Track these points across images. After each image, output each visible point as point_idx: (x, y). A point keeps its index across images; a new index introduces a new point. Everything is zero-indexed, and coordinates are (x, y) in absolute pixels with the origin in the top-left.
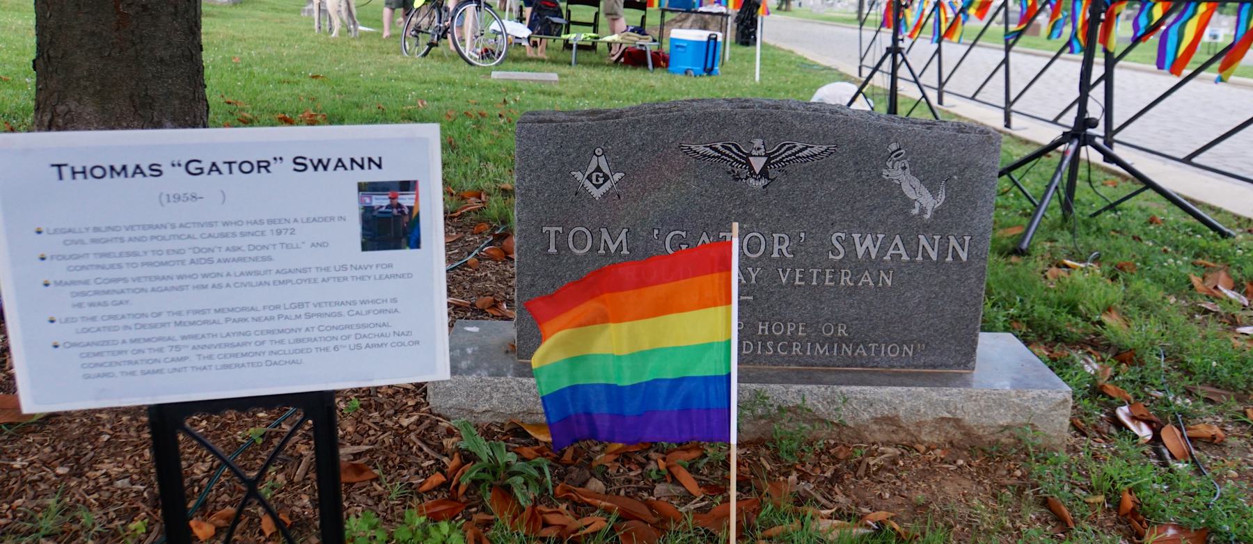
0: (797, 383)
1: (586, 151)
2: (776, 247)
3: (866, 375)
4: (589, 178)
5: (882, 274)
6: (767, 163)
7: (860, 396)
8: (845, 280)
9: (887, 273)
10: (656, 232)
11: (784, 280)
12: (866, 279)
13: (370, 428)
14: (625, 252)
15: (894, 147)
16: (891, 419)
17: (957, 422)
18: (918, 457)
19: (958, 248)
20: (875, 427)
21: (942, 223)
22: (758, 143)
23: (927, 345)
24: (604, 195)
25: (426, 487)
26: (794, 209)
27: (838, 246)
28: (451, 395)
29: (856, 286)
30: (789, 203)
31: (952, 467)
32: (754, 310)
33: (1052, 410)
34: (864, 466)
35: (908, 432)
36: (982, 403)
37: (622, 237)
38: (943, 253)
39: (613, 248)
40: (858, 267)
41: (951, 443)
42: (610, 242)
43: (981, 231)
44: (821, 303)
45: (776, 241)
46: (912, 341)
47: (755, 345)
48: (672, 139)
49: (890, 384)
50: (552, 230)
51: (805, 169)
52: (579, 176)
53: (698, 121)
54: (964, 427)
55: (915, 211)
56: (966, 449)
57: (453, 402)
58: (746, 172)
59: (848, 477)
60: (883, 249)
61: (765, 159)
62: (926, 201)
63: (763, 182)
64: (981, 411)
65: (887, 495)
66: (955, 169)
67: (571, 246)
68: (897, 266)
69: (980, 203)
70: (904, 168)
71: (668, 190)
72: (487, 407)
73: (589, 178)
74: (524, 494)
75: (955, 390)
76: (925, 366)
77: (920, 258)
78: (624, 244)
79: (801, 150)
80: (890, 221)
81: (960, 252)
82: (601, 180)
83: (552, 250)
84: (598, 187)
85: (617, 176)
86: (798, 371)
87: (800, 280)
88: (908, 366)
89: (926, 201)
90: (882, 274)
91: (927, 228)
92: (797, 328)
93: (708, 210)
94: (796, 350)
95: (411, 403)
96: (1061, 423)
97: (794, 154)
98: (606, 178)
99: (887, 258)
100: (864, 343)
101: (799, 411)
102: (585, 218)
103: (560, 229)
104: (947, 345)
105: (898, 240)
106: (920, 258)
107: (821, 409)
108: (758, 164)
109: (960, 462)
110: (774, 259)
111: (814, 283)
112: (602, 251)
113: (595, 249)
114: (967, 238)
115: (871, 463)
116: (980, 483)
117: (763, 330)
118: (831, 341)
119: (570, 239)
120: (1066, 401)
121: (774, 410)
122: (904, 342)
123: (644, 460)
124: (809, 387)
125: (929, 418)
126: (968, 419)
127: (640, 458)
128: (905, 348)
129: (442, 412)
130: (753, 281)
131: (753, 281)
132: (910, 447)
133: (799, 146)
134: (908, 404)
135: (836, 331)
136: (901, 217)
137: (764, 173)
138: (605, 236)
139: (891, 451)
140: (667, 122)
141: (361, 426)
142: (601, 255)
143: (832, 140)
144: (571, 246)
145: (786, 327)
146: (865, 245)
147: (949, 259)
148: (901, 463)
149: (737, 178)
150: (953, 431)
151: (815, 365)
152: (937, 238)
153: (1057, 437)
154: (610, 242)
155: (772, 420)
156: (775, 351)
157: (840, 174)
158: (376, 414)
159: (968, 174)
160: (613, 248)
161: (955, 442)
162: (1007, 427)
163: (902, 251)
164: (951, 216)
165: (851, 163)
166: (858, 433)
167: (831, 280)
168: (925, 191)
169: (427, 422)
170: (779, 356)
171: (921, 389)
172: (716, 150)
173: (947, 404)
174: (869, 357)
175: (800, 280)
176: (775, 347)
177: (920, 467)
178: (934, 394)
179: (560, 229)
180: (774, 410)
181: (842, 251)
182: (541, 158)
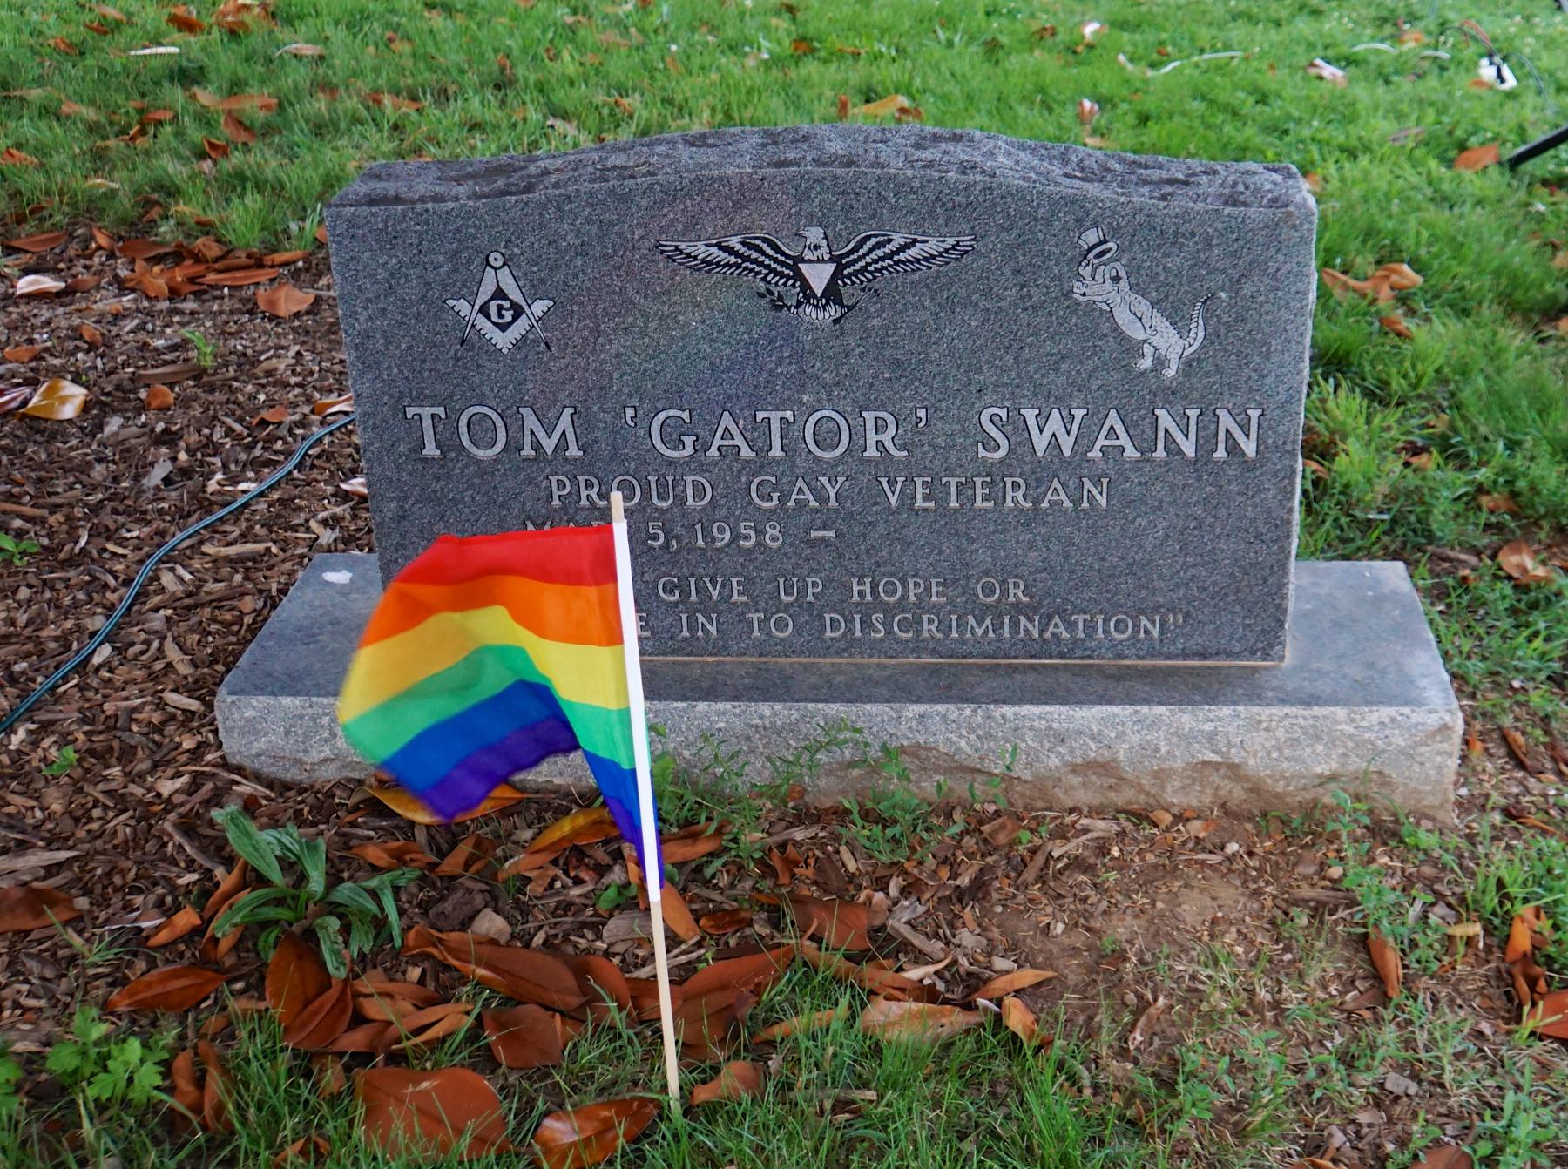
0: (918, 701)
1: (470, 260)
2: (872, 438)
3: (1064, 678)
4: (484, 311)
5: (1088, 484)
6: (836, 276)
7: (1040, 725)
8: (1015, 498)
9: (1097, 482)
10: (630, 412)
11: (893, 500)
12: (1057, 495)
13: (96, 803)
14: (573, 451)
15: (1092, 237)
16: (1103, 766)
17: (1234, 771)
18: (1151, 840)
19: (1237, 433)
20: (1076, 780)
21: (1199, 385)
22: (814, 235)
23: (1187, 615)
24: (519, 344)
25: (163, 937)
26: (899, 364)
27: (994, 433)
28: (256, 733)
29: (1036, 509)
30: (888, 352)
31: (1214, 859)
32: (840, 556)
33: (1416, 745)
34: (1040, 859)
35: (1140, 789)
36: (1281, 733)
37: (565, 422)
38: (1206, 445)
39: (549, 445)
40: (1039, 474)
41: (1223, 805)
42: (541, 434)
43: (1282, 398)
44: (972, 541)
45: (870, 425)
46: (1156, 609)
47: (849, 621)
48: (638, 233)
49: (1104, 700)
50: (426, 412)
51: (914, 284)
52: (463, 307)
53: (689, 196)
54: (1247, 779)
55: (1146, 363)
56: (1251, 818)
57: (261, 744)
58: (793, 294)
59: (1001, 886)
60: (1085, 438)
61: (831, 267)
62: (1166, 344)
63: (833, 311)
64: (1280, 750)
65: (1060, 927)
66: (1221, 279)
67: (466, 442)
68: (1114, 469)
69: (1275, 344)
70: (1116, 279)
71: (643, 333)
72: (327, 752)
73: (484, 311)
74: (336, 953)
75: (1226, 711)
76: (1185, 655)
77: (1160, 453)
78: (570, 436)
79: (903, 248)
80: (1095, 385)
81: (1242, 440)
82: (508, 316)
83: (431, 450)
84: (503, 328)
85: (540, 307)
86: (934, 671)
87: (925, 498)
88: (1152, 656)
89: (1166, 344)
90: (1088, 484)
91: (1169, 395)
92: (928, 589)
93: (729, 369)
94: (930, 629)
95: (188, 744)
96: (1439, 768)
97: (890, 256)
98: (518, 312)
99: (1095, 454)
100: (1061, 613)
101: (923, 754)
102: (486, 389)
103: (440, 411)
104: (1226, 617)
105: (1113, 419)
106: (1160, 453)
107: (965, 746)
108: (818, 276)
109: (1233, 847)
110: (870, 460)
111: (954, 504)
112: (528, 451)
113: (513, 446)
114: (1254, 414)
115: (1056, 854)
116: (1257, 893)
117: (861, 593)
118: (996, 611)
119: (463, 429)
120: (1445, 728)
121: (874, 753)
122: (1142, 612)
123: (607, 860)
124: (941, 708)
125: (1179, 764)
126: (1254, 764)
127: (601, 855)
128: (1144, 621)
129: (247, 763)
130: (833, 503)
131: (833, 503)
132: (1141, 817)
133: (899, 240)
134: (1135, 739)
135: (1005, 593)
136: (1118, 376)
137: (832, 294)
138: (531, 422)
139: (1101, 827)
140: (626, 198)
141: (80, 799)
142: (527, 459)
143: (966, 227)
144: (466, 442)
145: (905, 587)
146: (1050, 432)
147: (1221, 454)
148: (1115, 852)
149: (778, 305)
150: (1227, 785)
151: (970, 655)
152: (1193, 413)
153: (1432, 793)
154: (541, 434)
155: (874, 769)
156: (889, 632)
157: (985, 294)
158: (116, 771)
159: (1248, 289)
160: (549, 445)
161: (1231, 805)
162: (1333, 777)
163: (1124, 440)
164: (1219, 370)
165: (1007, 272)
166: (1042, 786)
167: (985, 499)
168: (1161, 323)
169: (209, 786)
170: (898, 641)
171: (1160, 709)
172: (731, 251)
173: (1211, 737)
174: (1075, 641)
175: (925, 498)
176: (887, 624)
177: (1150, 858)
178: (1186, 718)
179: (440, 411)
180: (874, 753)
181: (1004, 443)
182: (382, 275)
